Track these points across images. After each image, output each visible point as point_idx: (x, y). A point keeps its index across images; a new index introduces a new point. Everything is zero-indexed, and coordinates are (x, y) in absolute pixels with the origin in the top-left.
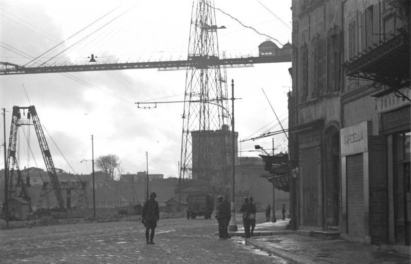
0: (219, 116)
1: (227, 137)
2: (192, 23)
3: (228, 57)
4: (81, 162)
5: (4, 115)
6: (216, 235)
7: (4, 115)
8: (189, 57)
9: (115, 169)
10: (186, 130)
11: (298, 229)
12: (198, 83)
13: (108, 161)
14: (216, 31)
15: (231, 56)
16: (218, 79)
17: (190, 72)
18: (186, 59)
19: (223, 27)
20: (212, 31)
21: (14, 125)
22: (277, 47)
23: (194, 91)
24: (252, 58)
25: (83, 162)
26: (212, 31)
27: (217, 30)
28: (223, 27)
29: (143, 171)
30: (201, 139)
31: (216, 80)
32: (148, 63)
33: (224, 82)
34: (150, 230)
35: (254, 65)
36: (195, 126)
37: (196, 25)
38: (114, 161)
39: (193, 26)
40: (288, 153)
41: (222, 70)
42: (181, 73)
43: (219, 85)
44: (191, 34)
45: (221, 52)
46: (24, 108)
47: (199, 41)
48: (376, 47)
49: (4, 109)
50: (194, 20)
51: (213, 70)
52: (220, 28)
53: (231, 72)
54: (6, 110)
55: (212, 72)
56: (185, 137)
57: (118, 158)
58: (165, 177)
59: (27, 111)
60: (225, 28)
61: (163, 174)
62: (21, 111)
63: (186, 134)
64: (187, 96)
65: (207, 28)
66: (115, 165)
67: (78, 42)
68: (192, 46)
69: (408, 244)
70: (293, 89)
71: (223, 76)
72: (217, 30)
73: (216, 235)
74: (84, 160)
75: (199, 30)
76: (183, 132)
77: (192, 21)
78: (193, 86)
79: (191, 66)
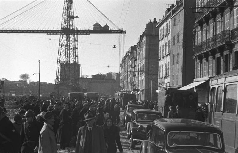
0: (74, 56)
1: (76, 66)
2: (63, 13)
3: (79, 29)
8: (61, 28)
9: (28, 80)
10: (59, 61)
13: (25, 76)
14: (74, 19)
15: (80, 29)
16: (74, 39)
17: (61, 36)
18: (60, 29)
19: (77, 17)
20: (72, 19)
22: (101, 26)
24: (89, 30)
26: (72, 19)
27: (75, 18)
28: (77, 17)
29: (97, 74)
31: (73, 40)
32: (43, 31)
33: (76, 41)
34: (218, 124)
35: (91, 34)
36: (63, 59)
37: (65, 14)
38: (28, 76)
39: (64, 15)
40: (120, 72)
41: (76, 36)
42: (57, 37)
45: (76, 27)
47: (66, 22)
48: (234, 5)
50: (64, 12)
51: (72, 35)
52: (75, 17)
53: (80, 37)
55: (71, 36)
57: (29, 75)
58: (48, 83)
61: (46, 82)
63: (59, 63)
65: (70, 17)
66: (28, 78)
67: (39, 4)
71: (76, 38)
72: (75, 18)
75: (66, 17)
78: (63, 41)
79: (62, 33)
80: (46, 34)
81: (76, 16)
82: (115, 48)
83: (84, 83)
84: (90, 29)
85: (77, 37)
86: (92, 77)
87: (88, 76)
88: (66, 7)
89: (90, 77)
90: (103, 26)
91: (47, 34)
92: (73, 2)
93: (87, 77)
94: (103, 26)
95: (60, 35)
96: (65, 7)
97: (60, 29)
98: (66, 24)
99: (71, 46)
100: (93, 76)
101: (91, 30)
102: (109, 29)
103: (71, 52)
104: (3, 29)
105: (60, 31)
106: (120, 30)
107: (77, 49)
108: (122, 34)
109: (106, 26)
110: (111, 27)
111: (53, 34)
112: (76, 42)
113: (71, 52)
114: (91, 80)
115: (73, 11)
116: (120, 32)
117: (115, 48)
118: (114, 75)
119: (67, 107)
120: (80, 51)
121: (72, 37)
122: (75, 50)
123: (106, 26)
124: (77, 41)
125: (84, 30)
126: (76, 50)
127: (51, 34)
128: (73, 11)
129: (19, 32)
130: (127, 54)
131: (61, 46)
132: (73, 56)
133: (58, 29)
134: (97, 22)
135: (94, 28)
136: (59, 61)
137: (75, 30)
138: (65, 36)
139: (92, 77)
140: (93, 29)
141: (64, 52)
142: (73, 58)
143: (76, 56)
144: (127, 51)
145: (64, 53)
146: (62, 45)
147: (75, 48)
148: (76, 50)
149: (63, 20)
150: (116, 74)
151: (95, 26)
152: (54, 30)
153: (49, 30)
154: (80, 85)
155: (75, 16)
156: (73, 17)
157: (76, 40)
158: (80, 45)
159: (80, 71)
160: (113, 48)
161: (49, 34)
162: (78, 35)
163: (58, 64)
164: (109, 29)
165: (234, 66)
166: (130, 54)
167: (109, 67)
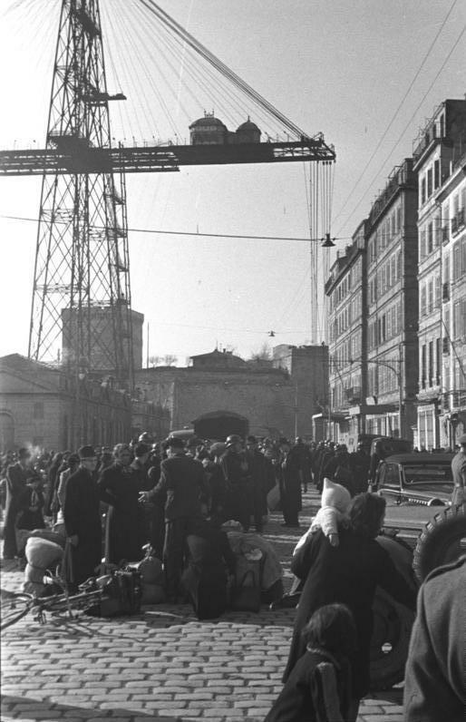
0: (110, 265)
8: (50, 138)
10: (41, 283)
11: (288, 372)
12: (65, 264)
14: (106, 105)
19: (120, 97)
23: (57, 279)
28: (120, 97)
29: (212, 350)
30: (77, 321)
35: (181, 167)
41: (117, 176)
44: (59, 55)
53: (136, 185)
55: (97, 182)
56: (38, 302)
60: (124, 98)
63: (41, 294)
68: (56, 116)
69: (5, 413)
72: (110, 102)
77: (56, 66)
81: (115, 94)
85: (123, 183)
86: (191, 365)
87: (175, 360)
88: (68, 48)
89: (182, 363)
90: (232, 128)
92: (99, 33)
93: (173, 364)
94: (232, 128)
96: (62, 47)
97: (41, 144)
98: (70, 122)
99: (98, 222)
100: (195, 359)
102: (263, 139)
103: (99, 251)
106: (312, 140)
108: (321, 162)
109: (249, 129)
110: (270, 131)
112: (118, 207)
113: (99, 251)
114: (186, 374)
115: (101, 70)
116: (316, 150)
118: (282, 356)
119: (125, 457)
120: (137, 248)
122: (116, 242)
123: (249, 129)
128: (101, 70)
130: (396, 178)
132: (105, 268)
134: (209, 111)
135: (195, 136)
136: (41, 283)
138: (65, 180)
139: (191, 365)
140: (188, 143)
141: (97, 269)
142: (108, 276)
143: (120, 267)
144: (400, 161)
145: (94, 264)
147: (116, 233)
149: (57, 103)
150: (291, 350)
151: (201, 129)
155: (111, 94)
156: (101, 99)
157: (116, 199)
159: (141, 340)
164: (263, 139)
165: (271, 356)
166: (438, 149)
167: (272, 335)
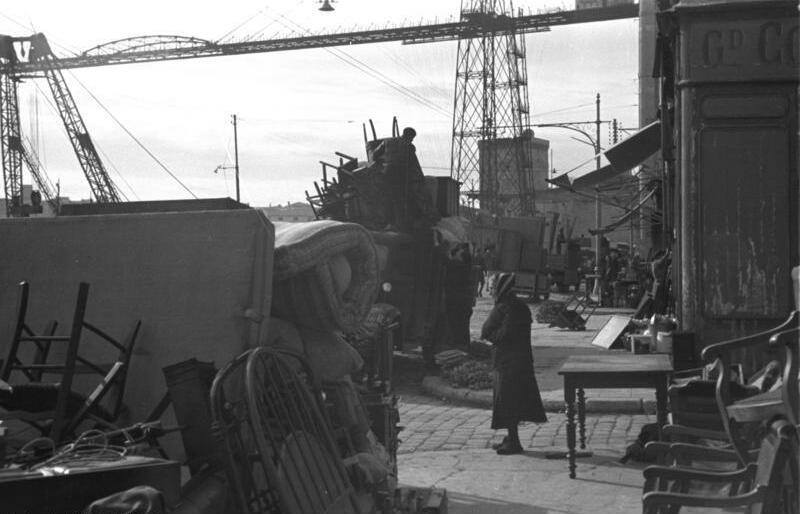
4: (216, 171)
5: (235, 124)
6: (488, 240)
7: (235, 124)
8: (462, 16)
12: (476, 114)
15: (530, 11)
18: (457, 20)
21: (11, 81)
25: (219, 171)
41: (518, 37)
42: (448, 47)
43: (513, 61)
46: (22, 40)
49: (235, 116)
53: (532, 40)
54: (237, 117)
55: (501, 41)
59: (27, 45)
62: (17, 46)
63: (458, 138)
64: (460, 78)
70: (481, 186)
73: (488, 240)
74: (219, 167)
76: (454, 134)
80: (400, 42)
82: (330, 9)
83: (560, 204)
84: (562, 9)
85: (523, 41)
91: (405, 44)
95: (456, 42)
99: (502, 77)
101: (568, 9)
104: (262, 40)
105: (455, 25)
107: (524, 83)
111: (424, 42)
117: (330, 9)
121: (505, 42)
124: (522, 56)
125: (542, 13)
126: (521, 87)
127: (540, 31)
129: (296, 44)
131: (463, 81)
132: (509, 112)
133: (452, 22)
137: (516, 15)
143: (522, 110)
146: (462, 132)
147: (518, 83)
148: (521, 87)
152: (440, 23)
153: (407, 29)
154: (538, 212)
158: (533, 70)
160: (322, 9)
161: (539, 28)
162: (526, 35)
163: (456, 143)
